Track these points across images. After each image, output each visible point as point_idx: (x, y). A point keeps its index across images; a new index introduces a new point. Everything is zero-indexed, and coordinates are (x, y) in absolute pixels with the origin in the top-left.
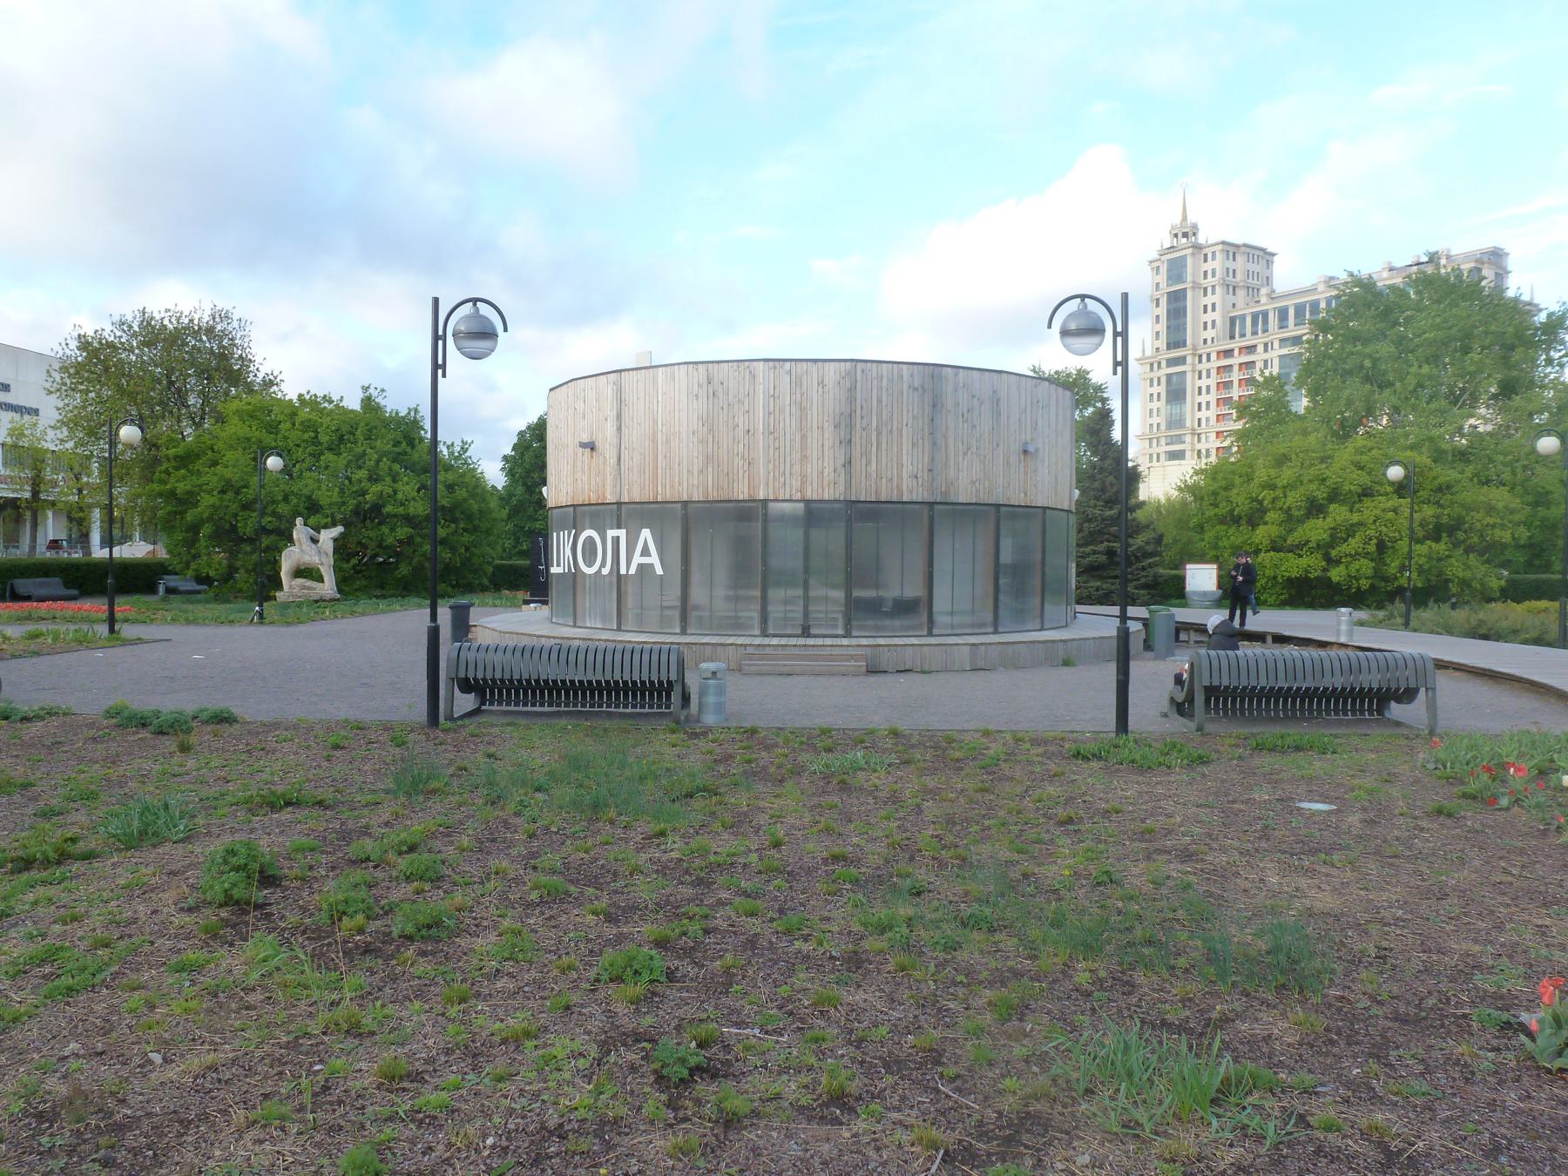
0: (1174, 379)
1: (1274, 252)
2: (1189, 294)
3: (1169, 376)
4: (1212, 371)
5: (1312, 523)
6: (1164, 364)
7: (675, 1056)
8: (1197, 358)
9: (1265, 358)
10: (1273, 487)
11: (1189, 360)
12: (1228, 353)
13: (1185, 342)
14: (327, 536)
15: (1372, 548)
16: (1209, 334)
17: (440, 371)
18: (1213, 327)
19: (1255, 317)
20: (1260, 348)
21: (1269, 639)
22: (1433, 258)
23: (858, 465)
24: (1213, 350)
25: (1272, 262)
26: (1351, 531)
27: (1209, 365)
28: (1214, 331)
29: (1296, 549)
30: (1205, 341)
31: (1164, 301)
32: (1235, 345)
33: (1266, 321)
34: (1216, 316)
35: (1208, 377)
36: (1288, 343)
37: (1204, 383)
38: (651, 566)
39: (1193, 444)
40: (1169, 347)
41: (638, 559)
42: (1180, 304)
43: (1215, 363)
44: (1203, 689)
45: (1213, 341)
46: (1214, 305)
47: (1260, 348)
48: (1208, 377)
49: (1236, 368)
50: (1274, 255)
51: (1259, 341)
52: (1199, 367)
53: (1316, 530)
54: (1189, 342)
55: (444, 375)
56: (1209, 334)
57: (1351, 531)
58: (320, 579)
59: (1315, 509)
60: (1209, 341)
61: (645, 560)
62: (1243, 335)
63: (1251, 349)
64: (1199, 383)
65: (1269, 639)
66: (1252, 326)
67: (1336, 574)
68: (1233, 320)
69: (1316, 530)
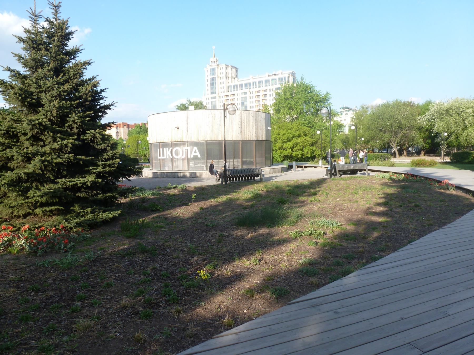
0: (213, 103)
2: (217, 79)
3: (212, 102)
5: (288, 143)
6: (210, 98)
10: (279, 134)
11: (217, 97)
12: (227, 96)
13: (216, 92)
15: (302, 148)
19: (234, 86)
21: (303, 167)
22: (396, 100)
23: (243, 132)
26: (297, 144)
29: (285, 149)
30: (221, 92)
31: (209, 80)
32: (229, 93)
33: (237, 88)
34: (224, 85)
36: (244, 94)
38: (197, 156)
40: (211, 94)
41: (193, 154)
49: (230, 100)
51: (236, 93)
53: (289, 145)
54: (217, 93)
56: (222, 90)
57: (297, 144)
59: (289, 140)
61: (195, 154)
65: (303, 167)
67: (294, 154)
69: (289, 145)
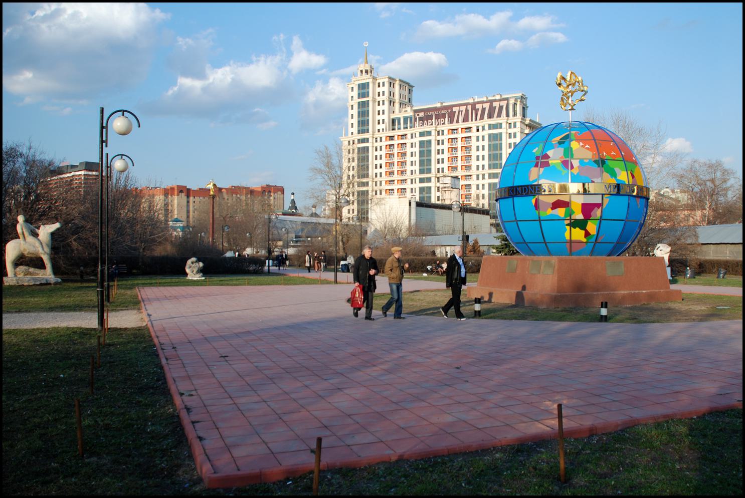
1: (413, 85)
4: (383, 182)
7: (568, 484)
8: (374, 183)
9: (412, 178)
14: (46, 231)
16: (381, 126)
17: (104, 144)
18: (383, 123)
20: (409, 136)
24: (383, 135)
25: (412, 90)
27: (381, 179)
28: (384, 125)
32: (396, 133)
34: (385, 117)
35: (381, 150)
37: (378, 153)
39: (373, 143)
42: (366, 109)
43: (384, 143)
44: (415, 203)
45: (383, 131)
46: (383, 111)
47: (409, 136)
48: (381, 150)
50: (413, 87)
52: (375, 188)
55: (107, 146)
58: (42, 266)
60: (381, 130)
62: (399, 129)
63: (403, 136)
64: (375, 144)
66: (404, 124)
68: (393, 121)
